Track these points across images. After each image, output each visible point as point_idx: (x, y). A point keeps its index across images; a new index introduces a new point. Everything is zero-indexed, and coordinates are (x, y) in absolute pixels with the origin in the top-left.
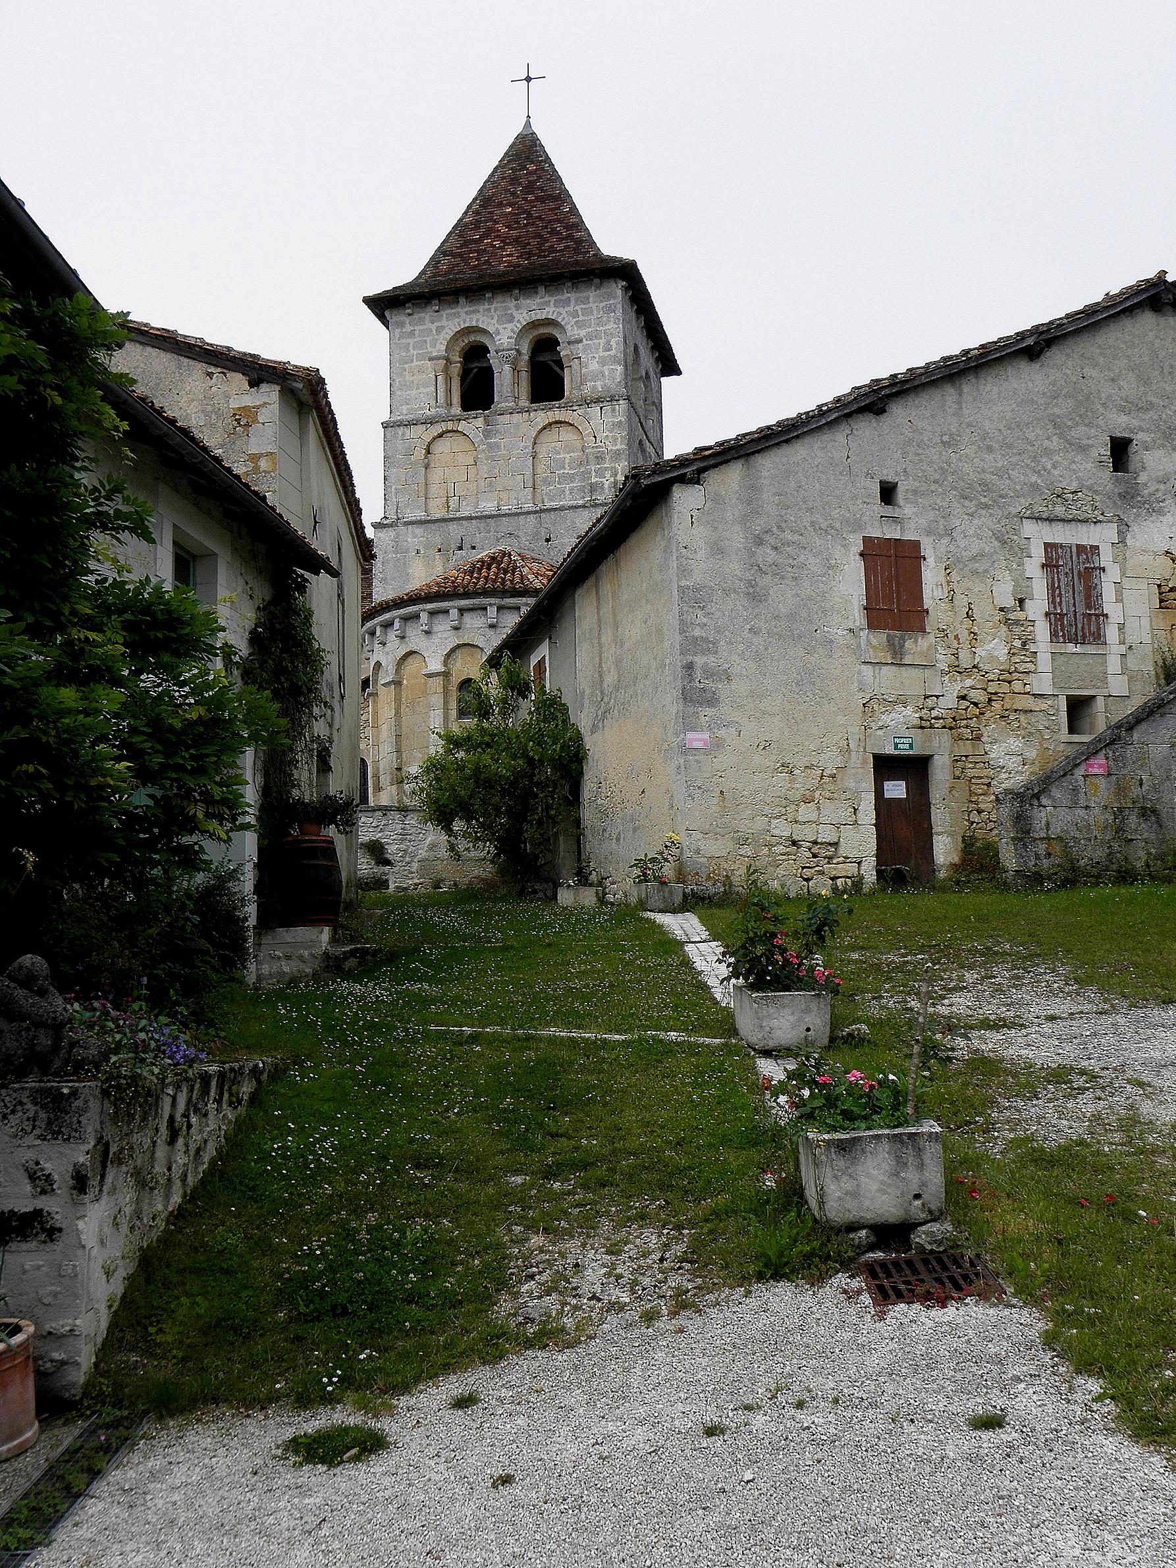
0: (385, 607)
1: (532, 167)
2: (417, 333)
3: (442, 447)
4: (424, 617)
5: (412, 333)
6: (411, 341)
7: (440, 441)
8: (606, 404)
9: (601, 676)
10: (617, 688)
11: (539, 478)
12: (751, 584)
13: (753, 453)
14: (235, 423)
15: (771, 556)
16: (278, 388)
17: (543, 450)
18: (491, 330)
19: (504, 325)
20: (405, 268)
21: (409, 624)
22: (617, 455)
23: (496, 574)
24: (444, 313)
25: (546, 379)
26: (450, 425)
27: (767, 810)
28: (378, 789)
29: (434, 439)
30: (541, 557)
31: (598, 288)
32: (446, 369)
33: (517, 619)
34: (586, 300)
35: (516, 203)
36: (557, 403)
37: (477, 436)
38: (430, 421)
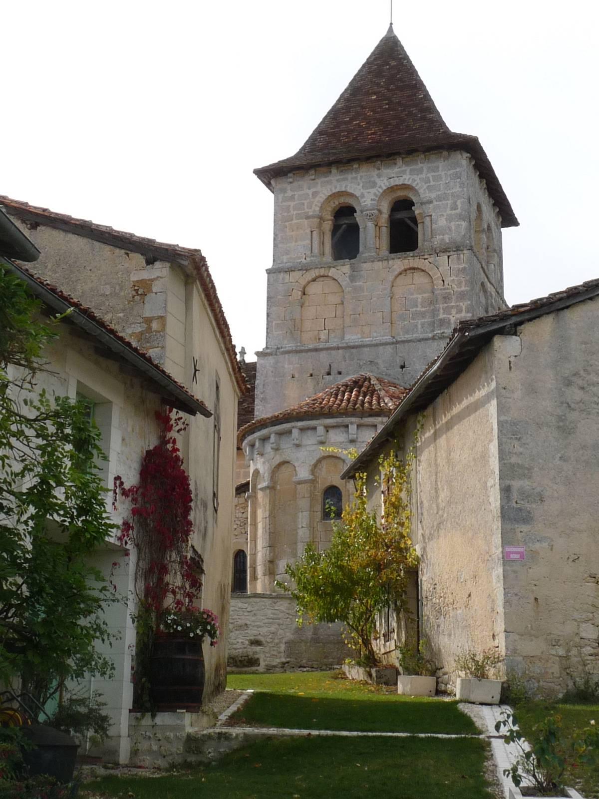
0: (264, 424)
1: (393, 63)
2: (296, 197)
3: (314, 289)
4: (295, 432)
5: (292, 198)
6: (292, 204)
7: (315, 284)
8: (452, 253)
9: (436, 492)
10: (449, 503)
11: (395, 315)
12: (560, 418)
13: (563, 309)
14: (134, 293)
15: (578, 395)
16: (168, 265)
17: (399, 291)
18: (357, 194)
19: (369, 189)
20: (288, 144)
21: (284, 438)
22: (462, 296)
23: (357, 396)
24: (319, 181)
25: (404, 234)
26: (322, 272)
27: (576, 615)
28: (254, 578)
29: (309, 282)
30: (396, 381)
31: (446, 159)
32: (320, 226)
33: (383, 426)
34: (436, 169)
35: (380, 92)
36: (411, 254)
37: (345, 281)
38: (306, 269)
